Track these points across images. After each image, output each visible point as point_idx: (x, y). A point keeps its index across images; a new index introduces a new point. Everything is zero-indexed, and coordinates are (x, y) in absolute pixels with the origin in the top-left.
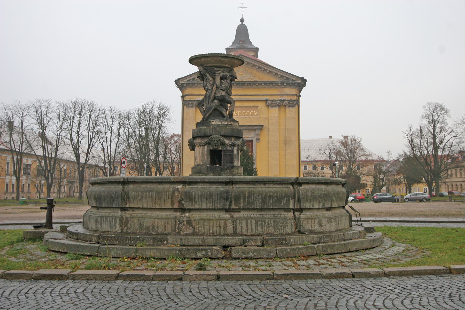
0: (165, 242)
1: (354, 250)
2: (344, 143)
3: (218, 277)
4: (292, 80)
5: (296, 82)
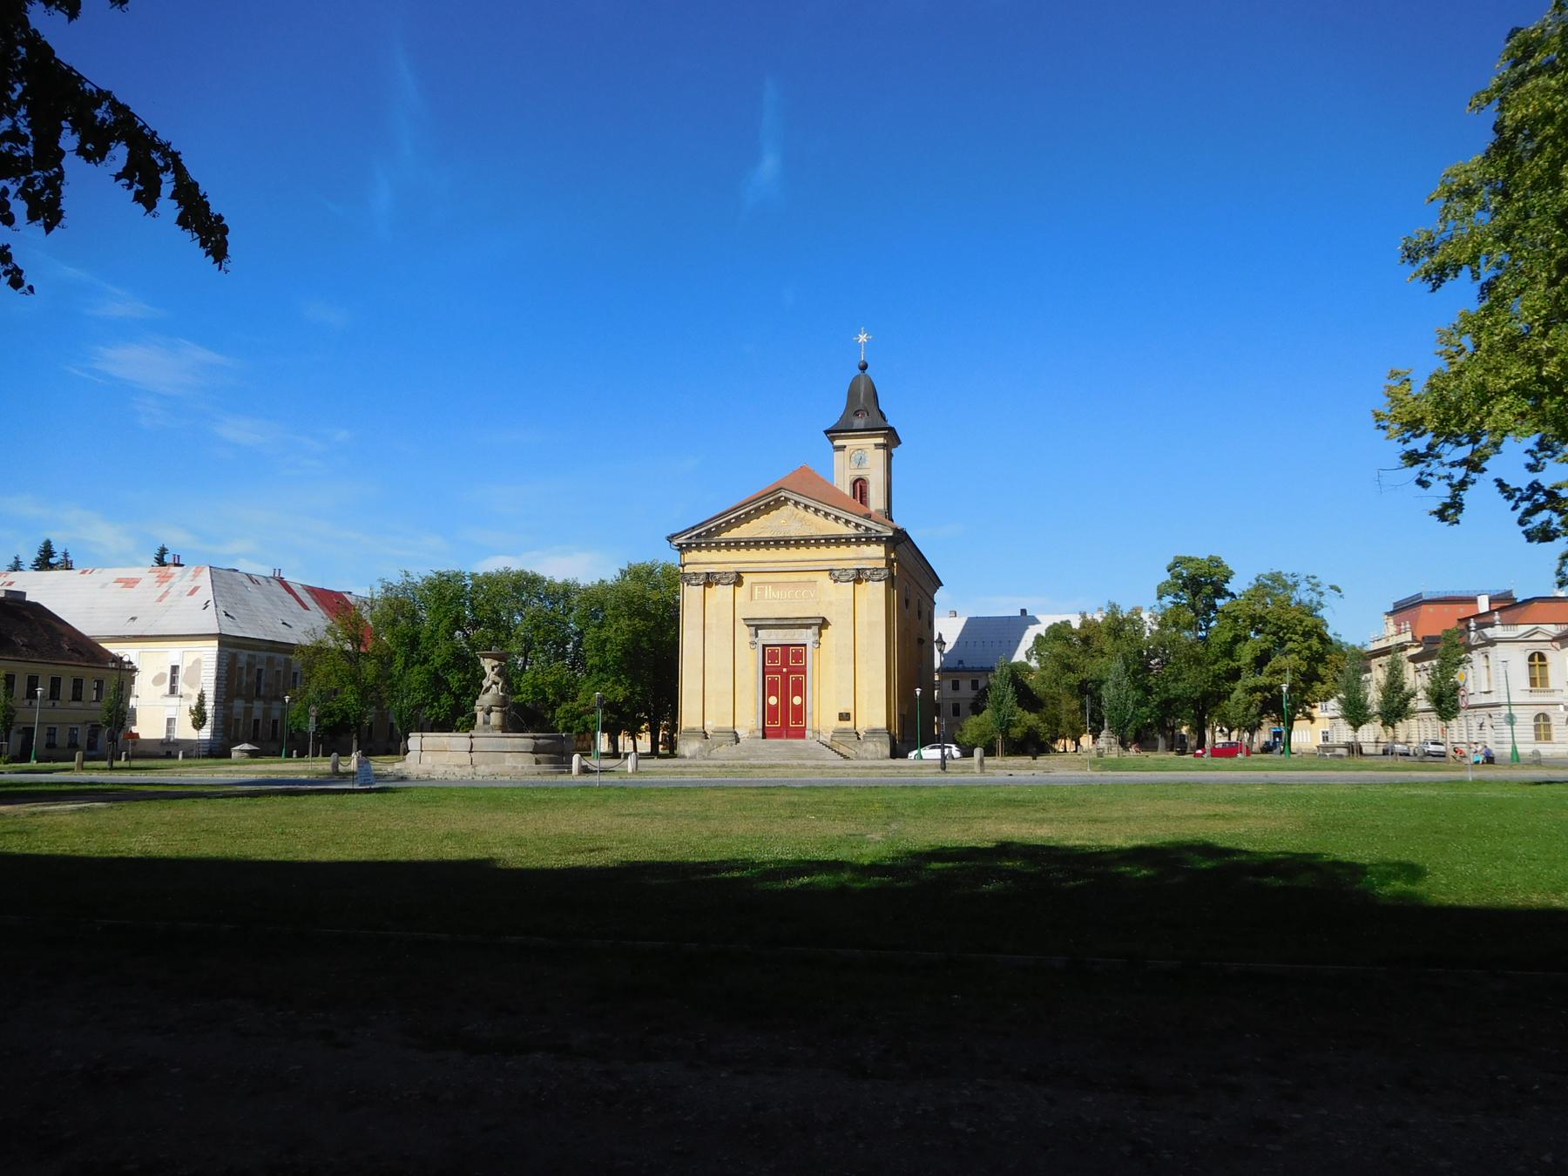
0: (1335, 880)
1: (841, 752)
2: (1530, 59)
3: (1498, 449)
4: (877, 531)
5: (883, 535)
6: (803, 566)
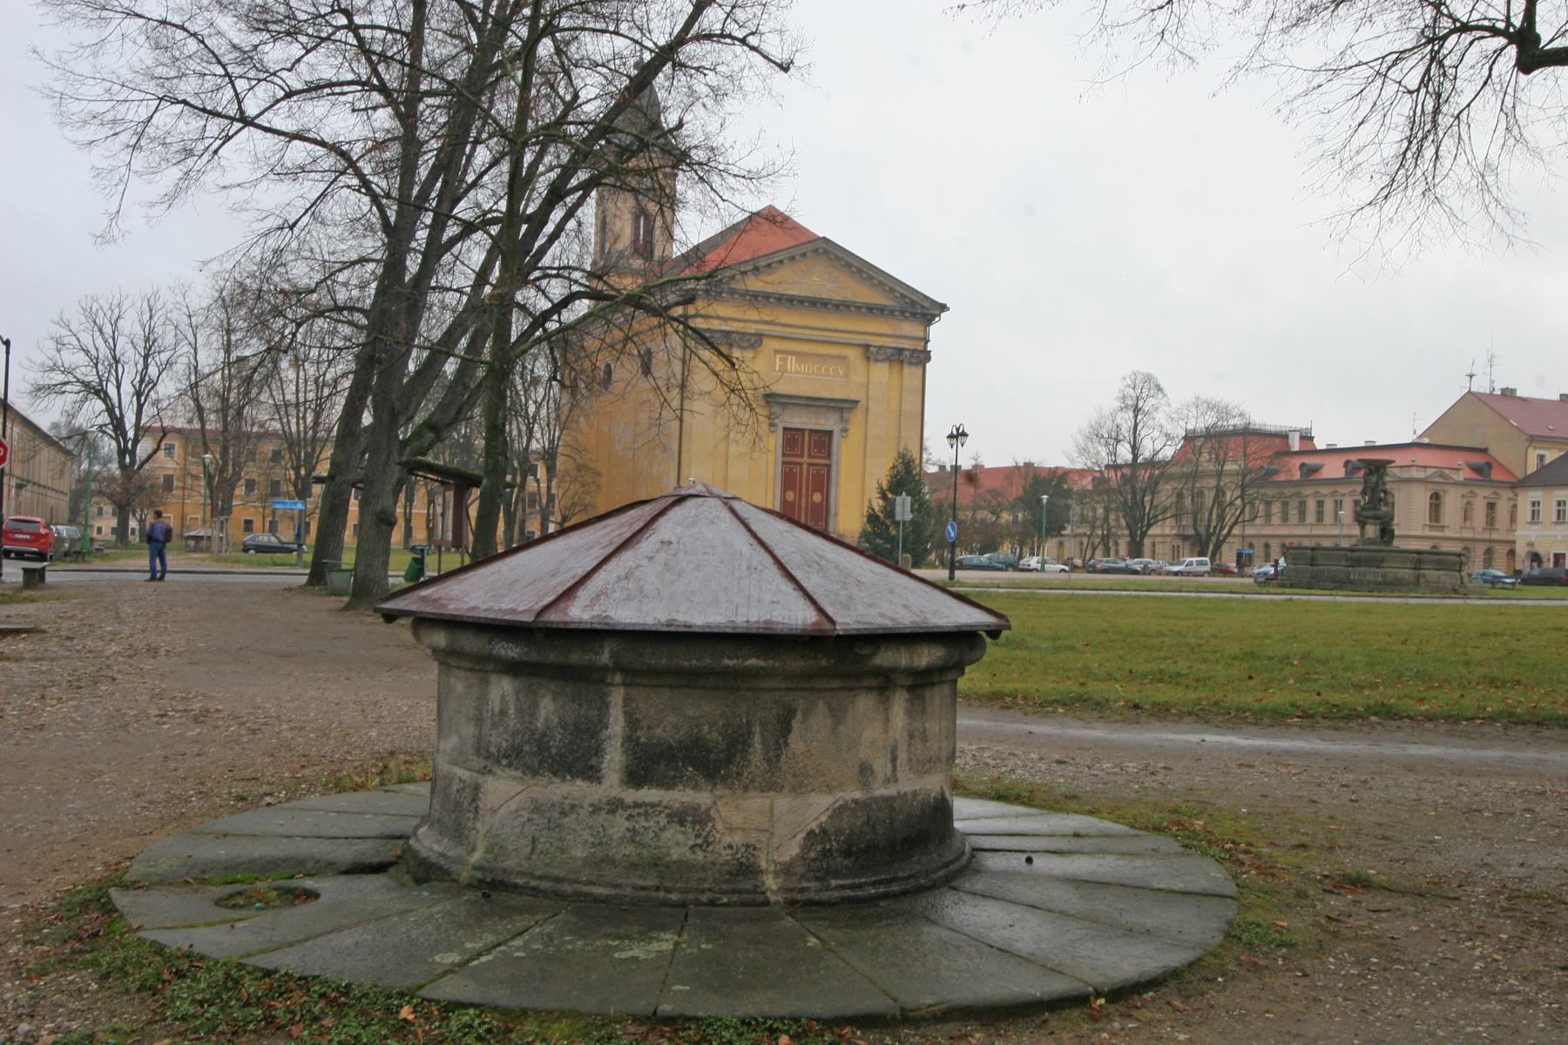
6: (807, 333)
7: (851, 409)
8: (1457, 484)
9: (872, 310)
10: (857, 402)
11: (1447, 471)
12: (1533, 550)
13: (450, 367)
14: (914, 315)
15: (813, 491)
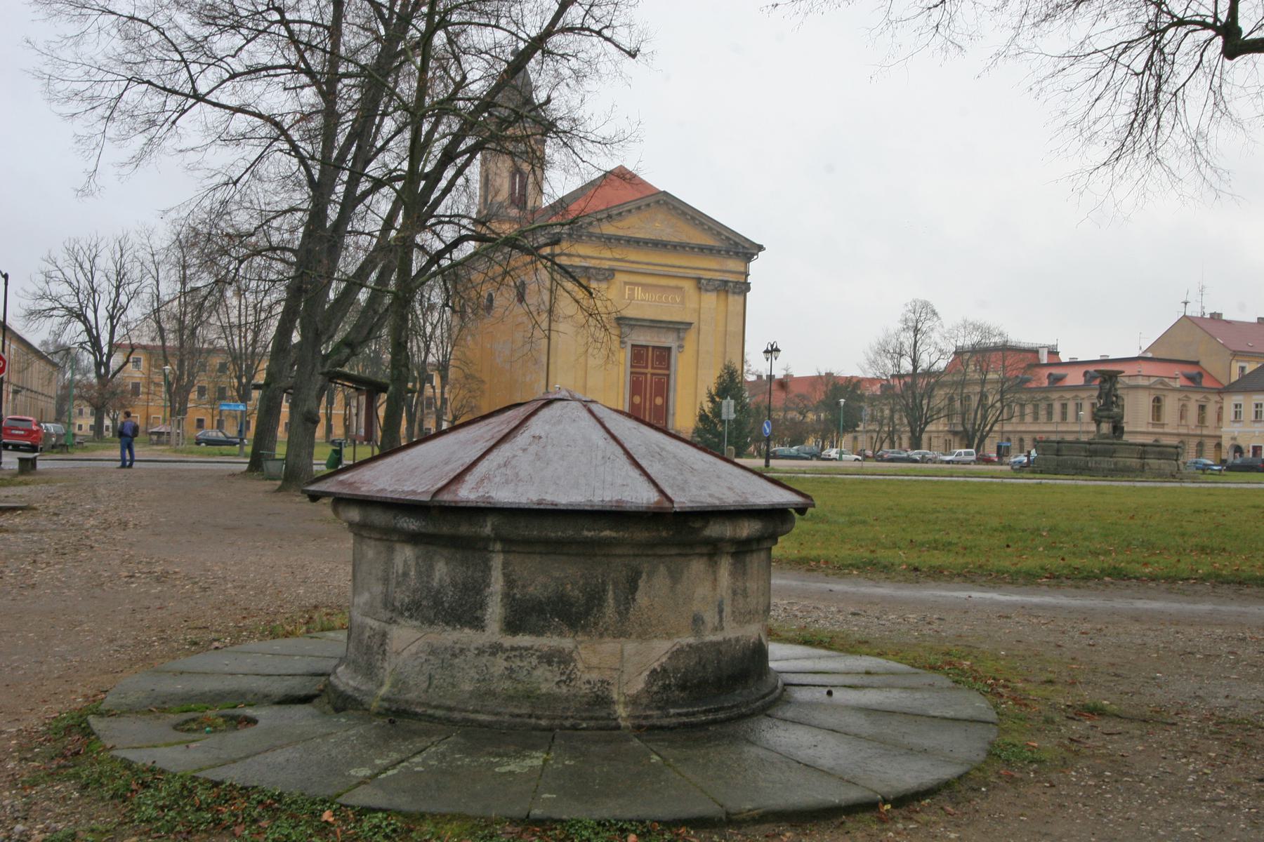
6: (651, 269)
7: (686, 330)
8: (1174, 390)
9: (703, 250)
10: (691, 324)
11: (1166, 380)
12: (1236, 443)
13: (363, 296)
14: (737, 254)
15: (656, 396)
